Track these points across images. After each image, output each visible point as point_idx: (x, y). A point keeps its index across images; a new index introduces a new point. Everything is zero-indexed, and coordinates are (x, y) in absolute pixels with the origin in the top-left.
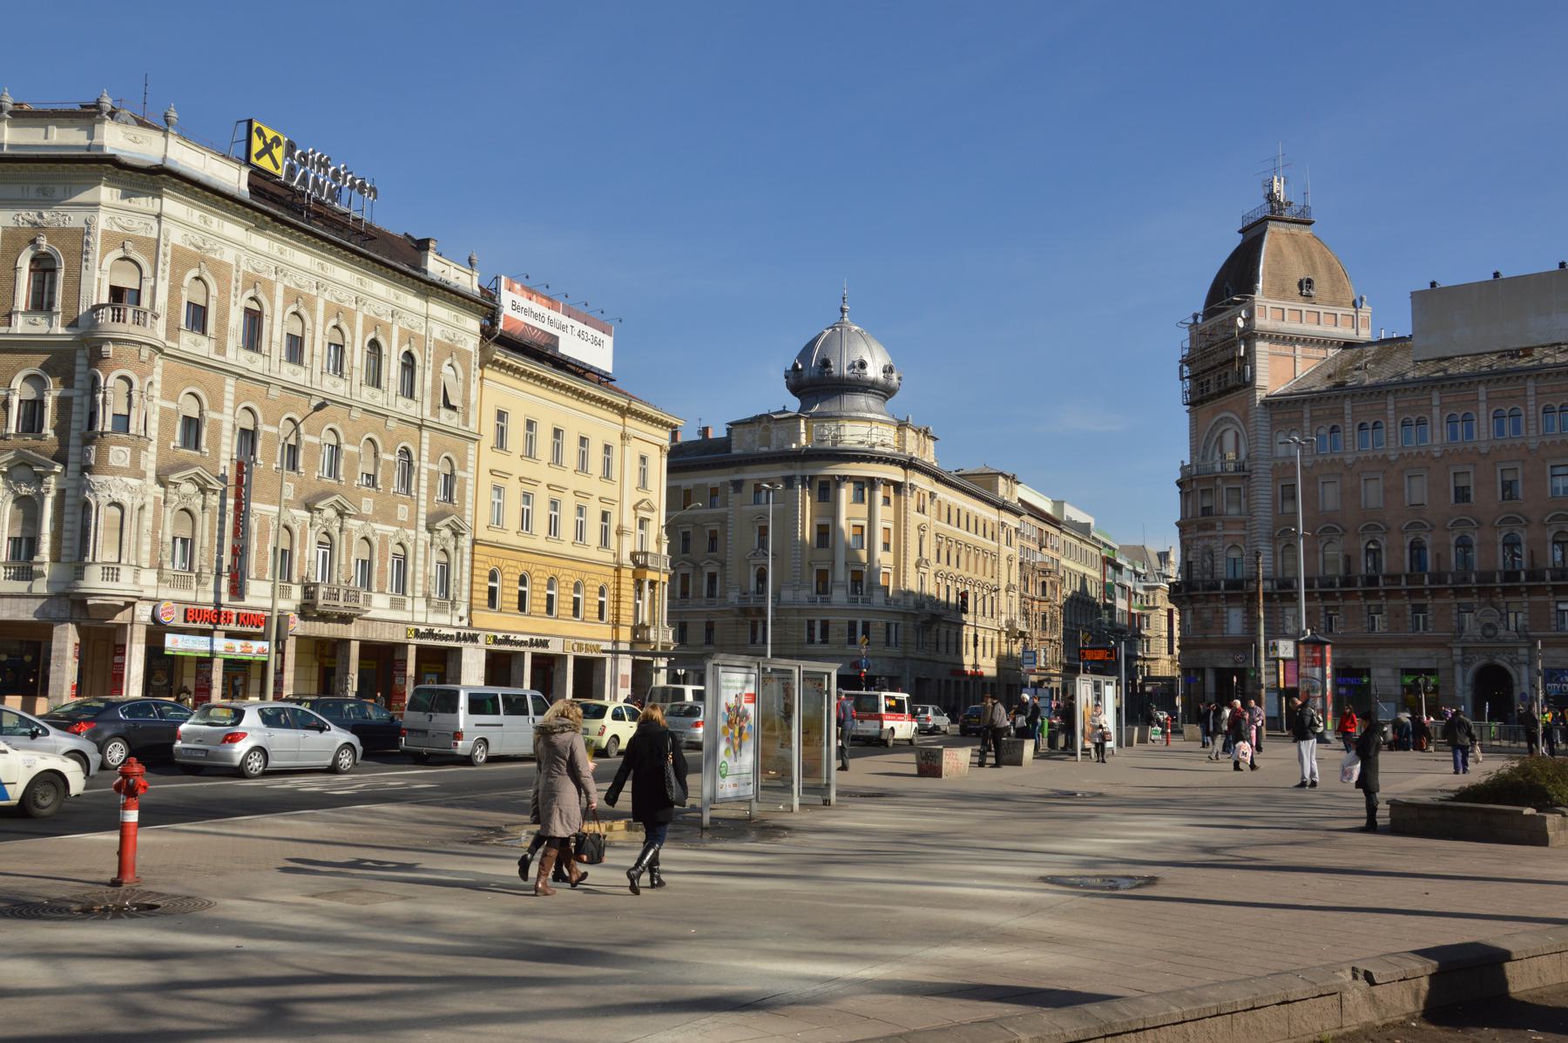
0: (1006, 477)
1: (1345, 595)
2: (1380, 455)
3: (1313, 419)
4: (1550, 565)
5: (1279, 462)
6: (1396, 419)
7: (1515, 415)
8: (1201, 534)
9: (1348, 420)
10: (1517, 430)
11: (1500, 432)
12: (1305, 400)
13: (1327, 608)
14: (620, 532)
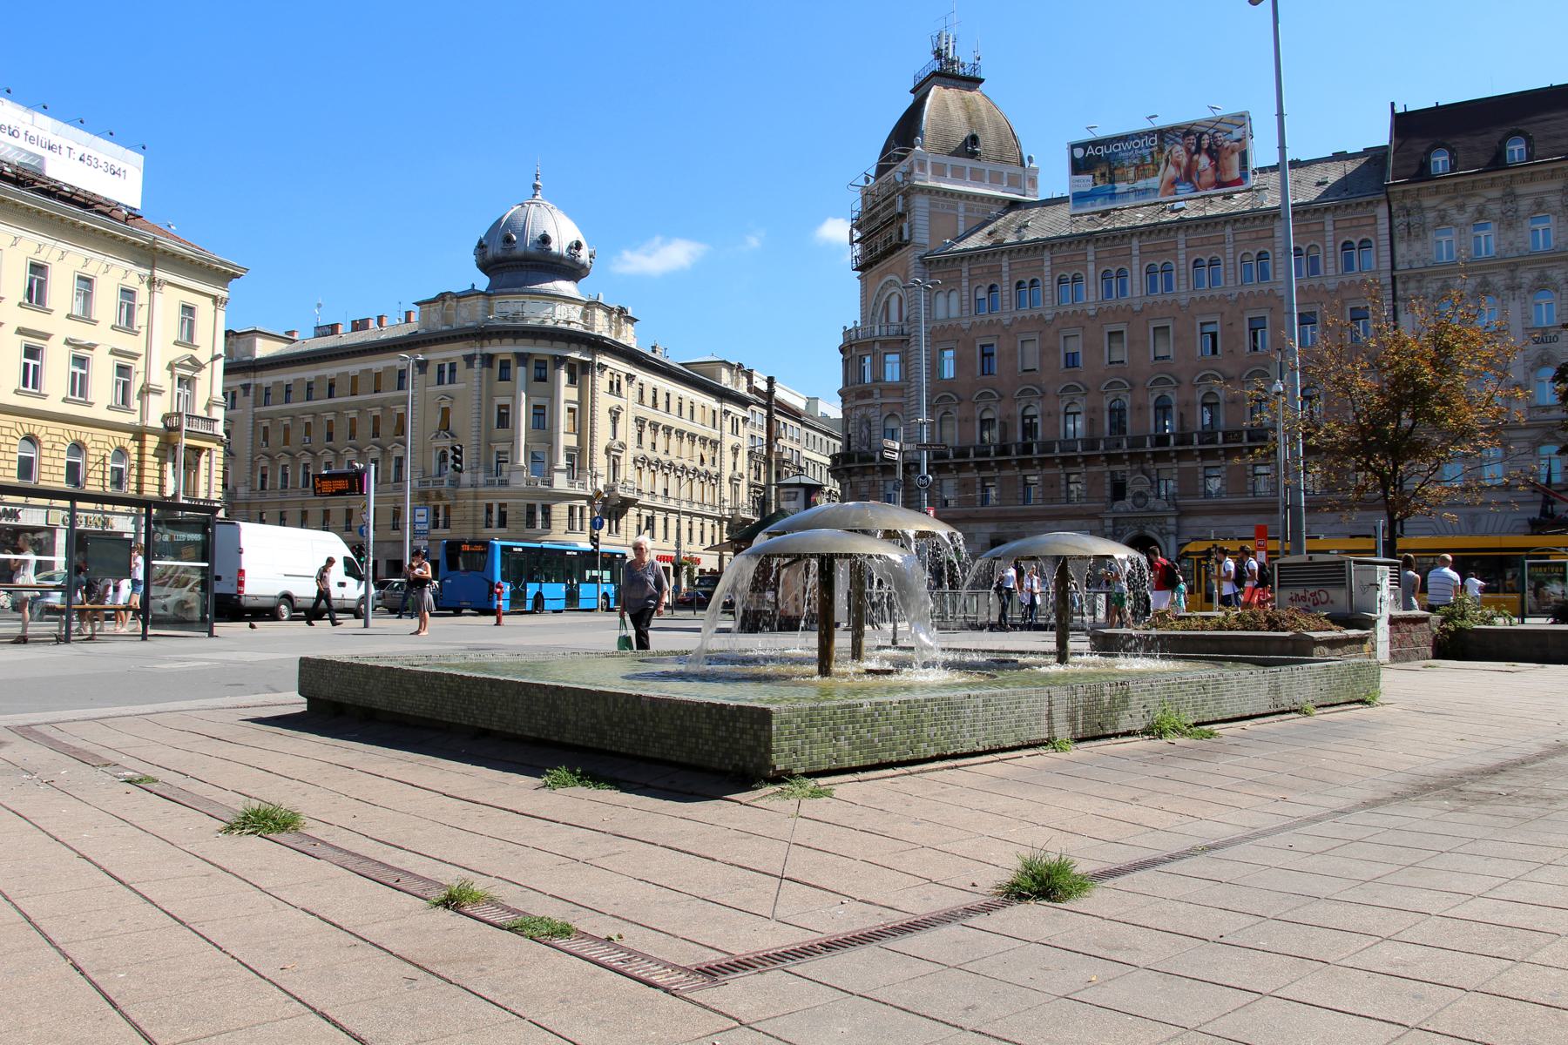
0: (730, 366)
1: (1001, 465)
2: (1036, 314)
3: (971, 278)
4: (1199, 428)
5: (938, 325)
6: (1053, 276)
7: (1167, 270)
8: (859, 402)
9: (1006, 278)
10: (1169, 287)
11: (1153, 287)
12: (963, 258)
13: (984, 480)
14: (146, 391)
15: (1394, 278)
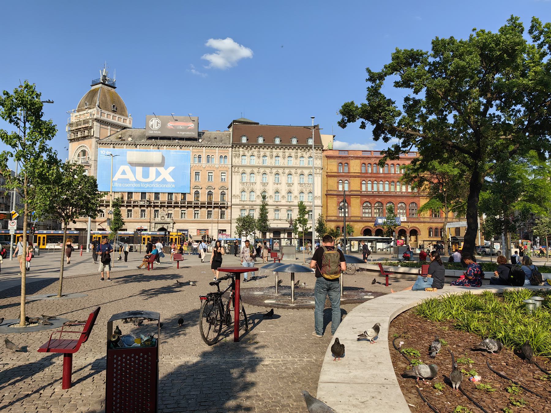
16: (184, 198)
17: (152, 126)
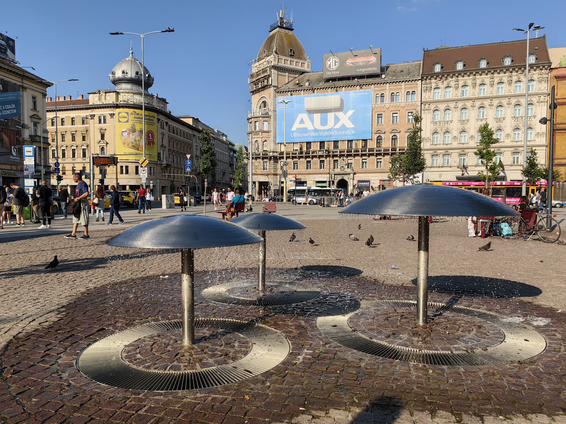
15: (421, 103)
16: (366, 145)
17: (330, 65)
